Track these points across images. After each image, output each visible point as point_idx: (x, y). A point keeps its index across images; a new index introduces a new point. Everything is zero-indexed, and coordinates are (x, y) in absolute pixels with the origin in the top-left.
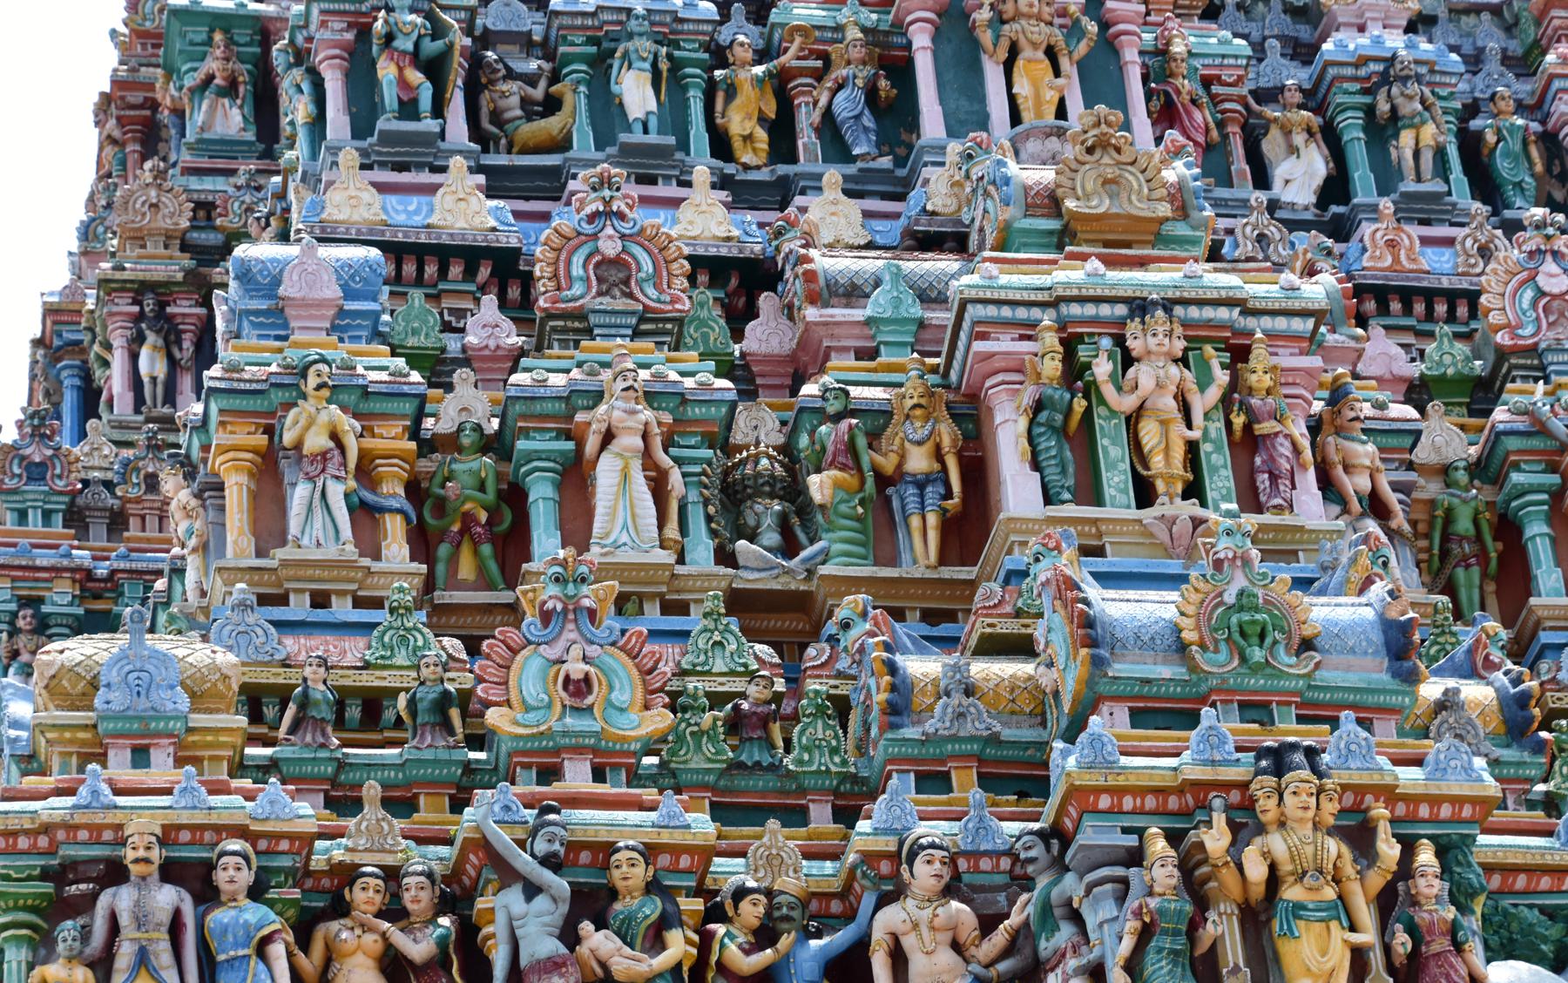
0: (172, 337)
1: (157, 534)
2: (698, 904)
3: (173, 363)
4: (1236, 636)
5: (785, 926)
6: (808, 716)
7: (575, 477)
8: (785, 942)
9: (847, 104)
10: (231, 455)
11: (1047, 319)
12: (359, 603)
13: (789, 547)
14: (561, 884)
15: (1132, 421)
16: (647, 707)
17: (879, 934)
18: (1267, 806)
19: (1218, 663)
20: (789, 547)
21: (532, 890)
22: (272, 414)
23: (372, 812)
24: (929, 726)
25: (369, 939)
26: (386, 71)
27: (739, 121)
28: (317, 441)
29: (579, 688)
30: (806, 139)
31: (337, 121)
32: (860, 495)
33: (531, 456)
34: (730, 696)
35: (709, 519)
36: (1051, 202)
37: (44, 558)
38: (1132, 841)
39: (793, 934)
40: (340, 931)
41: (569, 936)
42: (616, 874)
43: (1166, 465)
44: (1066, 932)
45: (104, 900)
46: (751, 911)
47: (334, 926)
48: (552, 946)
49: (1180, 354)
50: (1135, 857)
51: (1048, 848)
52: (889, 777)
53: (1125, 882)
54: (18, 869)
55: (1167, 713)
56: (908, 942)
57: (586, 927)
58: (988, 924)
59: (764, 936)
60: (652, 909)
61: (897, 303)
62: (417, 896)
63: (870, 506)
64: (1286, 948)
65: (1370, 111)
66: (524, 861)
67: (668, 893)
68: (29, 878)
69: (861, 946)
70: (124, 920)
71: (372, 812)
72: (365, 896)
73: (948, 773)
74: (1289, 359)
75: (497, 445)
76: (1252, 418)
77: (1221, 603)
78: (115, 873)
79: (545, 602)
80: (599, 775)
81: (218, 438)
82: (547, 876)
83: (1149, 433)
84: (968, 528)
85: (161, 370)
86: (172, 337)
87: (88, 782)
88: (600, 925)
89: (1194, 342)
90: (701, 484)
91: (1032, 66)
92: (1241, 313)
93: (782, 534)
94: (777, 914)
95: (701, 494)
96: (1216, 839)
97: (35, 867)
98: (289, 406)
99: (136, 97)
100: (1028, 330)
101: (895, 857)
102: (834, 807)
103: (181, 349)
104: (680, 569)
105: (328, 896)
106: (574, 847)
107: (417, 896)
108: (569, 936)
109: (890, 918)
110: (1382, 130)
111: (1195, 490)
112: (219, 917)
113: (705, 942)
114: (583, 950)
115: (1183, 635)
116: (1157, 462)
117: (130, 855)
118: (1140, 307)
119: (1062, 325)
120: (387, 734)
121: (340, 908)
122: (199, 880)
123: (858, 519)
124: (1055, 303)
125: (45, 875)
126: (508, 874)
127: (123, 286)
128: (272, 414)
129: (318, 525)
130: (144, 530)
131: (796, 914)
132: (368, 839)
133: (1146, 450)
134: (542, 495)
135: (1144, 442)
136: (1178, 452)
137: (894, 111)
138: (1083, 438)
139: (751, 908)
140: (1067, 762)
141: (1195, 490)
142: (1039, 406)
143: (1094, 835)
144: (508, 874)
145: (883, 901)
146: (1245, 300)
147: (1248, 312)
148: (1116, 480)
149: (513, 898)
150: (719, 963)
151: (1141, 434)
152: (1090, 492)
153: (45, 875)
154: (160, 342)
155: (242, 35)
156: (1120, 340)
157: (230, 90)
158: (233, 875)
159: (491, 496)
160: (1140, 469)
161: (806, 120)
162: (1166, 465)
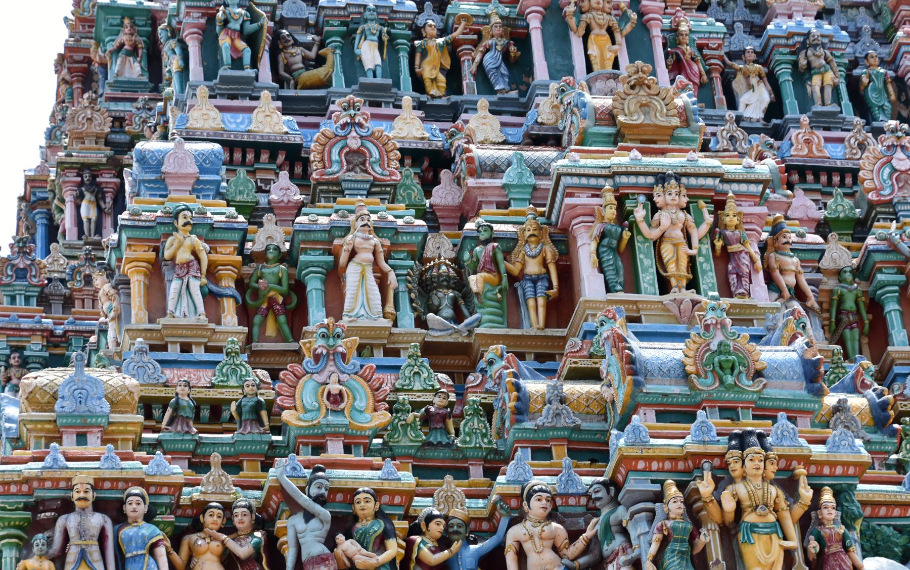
2: (405, 524)
4: (718, 369)
5: (456, 537)
6: (469, 415)
7: (334, 277)
8: (455, 546)
9: (491, 60)
10: (134, 264)
11: (608, 185)
12: (208, 350)
13: (458, 317)
14: (325, 513)
15: (657, 244)
16: (375, 410)
17: (510, 542)
18: (735, 468)
19: (707, 385)
20: (458, 317)
21: (309, 516)
22: (158, 240)
23: (216, 471)
24: (539, 421)
25: (214, 544)
26: (224, 41)
27: (429, 70)
28: (184, 256)
29: (336, 399)
30: (468, 80)
31: (196, 70)
32: (499, 287)
33: (308, 265)
34: (424, 404)
35: (411, 301)
36: (610, 117)
37: (26, 324)
38: (657, 487)
39: (460, 541)
41: (331, 543)
42: (358, 507)
43: (677, 270)
44: (619, 540)
45: (61, 522)
46: (436, 528)
47: (194, 537)
48: (320, 549)
49: (685, 205)
50: (659, 497)
51: (608, 492)
52: (516, 450)
53: (653, 511)
54: (10, 504)
55: (677, 413)
56: (527, 546)
57: (340, 537)
58: (573, 536)
59: (444, 543)
60: (378, 527)
61: (520, 175)
62: (242, 519)
63: (505, 293)
64: (746, 550)
65: (795, 64)
66: (304, 499)
67: (387, 518)
68: (17, 509)
69: (500, 549)
70: (72, 534)
71: (216, 471)
72: (212, 520)
73: (550, 448)
74: (748, 208)
75: (288, 258)
76: (727, 242)
77: (709, 350)
78: (67, 506)
79: (316, 349)
80: (347, 449)
81: (126, 254)
82: (318, 508)
83: (667, 251)
84: (562, 306)
87: (51, 453)
88: (348, 536)
89: (693, 199)
90: (407, 280)
91: (599, 38)
92: (720, 181)
93: (454, 310)
94: (451, 530)
95: (407, 286)
96: (706, 486)
97: (20, 503)
98: (168, 235)
99: (79, 56)
100: (597, 192)
101: (519, 497)
102: (484, 468)
104: (394, 330)
105: (191, 520)
106: (333, 491)
107: (242, 519)
108: (331, 543)
109: (517, 532)
110: (802, 75)
111: (693, 284)
112: (127, 532)
113: (409, 546)
114: (338, 551)
115: (687, 368)
116: (672, 268)
117: (76, 496)
118: (662, 178)
119: (616, 189)
120: (225, 426)
121: (197, 527)
122: (116, 511)
123: (498, 301)
124: (612, 176)
125: (26, 507)
126: (295, 507)
127: (71, 166)
128: (158, 240)
129: (184, 304)
131: (462, 530)
132: (213, 487)
133: (665, 261)
134: (314, 287)
135: (664, 256)
136: (684, 262)
137: (519, 65)
138: (629, 254)
139: (436, 526)
140: (619, 442)
141: (693, 284)
142: (603, 235)
143: (635, 484)
144: (295, 507)
145: (513, 522)
146: (723, 174)
147: (724, 181)
148: (648, 278)
149: (298, 521)
150: (417, 558)
151: (662, 252)
152: (633, 285)
153: (26, 507)
155: (141, 20)
156: (650, 197)
157: (134, 52)
158: (135, 508)
159: (285, 288)
160: (661, 272)
161: (468, 69)
162: (677, 270)
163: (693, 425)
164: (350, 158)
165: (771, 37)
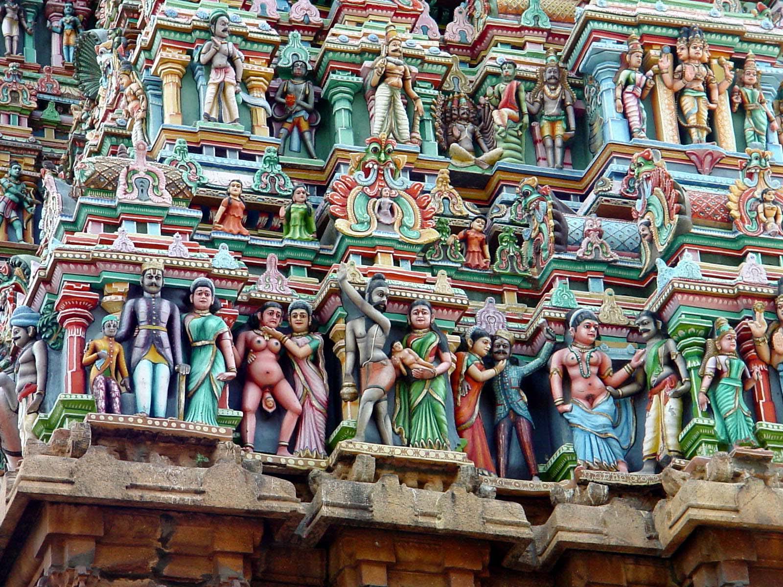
0: (22, 14)
1: (17, 127)
2: (457, 339)
3: (22, 29)
4: (762, 216)
5: (501, 356)
6: (505, 242)
8: (502, 364)
10: (169, 65)
11: (634, 32)
12: (242, 156)
13: (477, 150)
14: (386, 320)
16: (422, 227)
17: (554, 364)
20: (477, 150)
22: (192, 45)
23: (272, 270)
24: (579, 253)
25: (274, 342)
32: (520, 124)
33: (337, 84)
34: (461, 229)
35: (435, 129)
38: (708, 324)
39: (505, 360)
40: (259, 338)
42: (414, 317)
46: (483, 346)
47: (252, 334)
49: (706, 60)
51: (656, 324)
52: (554, 280)
53: (704, 346)
54: (78, 283)
56: (573, 372)
57: (398, 345)
59: (489, 361)
60: (434, 340)
61: (536, 18)
62: (300, 321)
63: (525, 131)
67: (440, 332)
68: (84, 289)
69: (544, 370)
70: (142, 316)
71: (272, 270)
72: (271, 318)
73: (587, 280)
74: (764, 68)
75: (314, 77)
77: (753, 197)
79: (366, 163)
80: (397, 262)
81: (159, 55)
82: (378, 314)
83: (688, 102)
85: (15, 32)
86: (22, 14)
87: (120, 237)
88: (407, 346)
90: (431, 109)
92: (740, 41)
93: (473, 143)
94: (496, 350)
95: (431, 115)
97: (87, 283)
98: (203, 41)
100: (623, 37)
101: (565, 323)
102: (518, 295)
103: (27, 22)
104: (421, 156)
105: (247, 318)
106: (392, 300)
107: (300, 321)
113: (459, 363)
114: (397, 358)
115: (732, 212)
116: (692, 120)
117: (147, 281)
119: (643, 36)
120: (260, 232)
121: (255, 324)
123: (519, 137)
124: (638, 25)
128: (192, 45)
130: (9, 124)
131: (507, 351)
132: (271, 285)
133: (686, 112)
135: (684, 108)
136: (705, 114)
139: (483, 345)
140: (666, 275)
146: (744, 33)
147: (743, 40)
150: (467, 373)
151: (683, 104)
154: (16, 17)
156: (673, 50)
159: (310, 106)
160: (682, 122)
163: (48, 532)
164: (13, 95)
165: (327, 50)
